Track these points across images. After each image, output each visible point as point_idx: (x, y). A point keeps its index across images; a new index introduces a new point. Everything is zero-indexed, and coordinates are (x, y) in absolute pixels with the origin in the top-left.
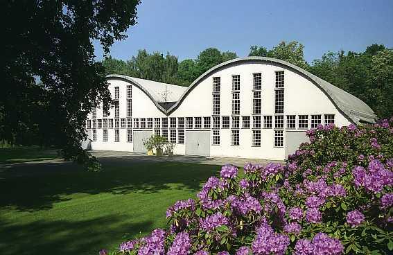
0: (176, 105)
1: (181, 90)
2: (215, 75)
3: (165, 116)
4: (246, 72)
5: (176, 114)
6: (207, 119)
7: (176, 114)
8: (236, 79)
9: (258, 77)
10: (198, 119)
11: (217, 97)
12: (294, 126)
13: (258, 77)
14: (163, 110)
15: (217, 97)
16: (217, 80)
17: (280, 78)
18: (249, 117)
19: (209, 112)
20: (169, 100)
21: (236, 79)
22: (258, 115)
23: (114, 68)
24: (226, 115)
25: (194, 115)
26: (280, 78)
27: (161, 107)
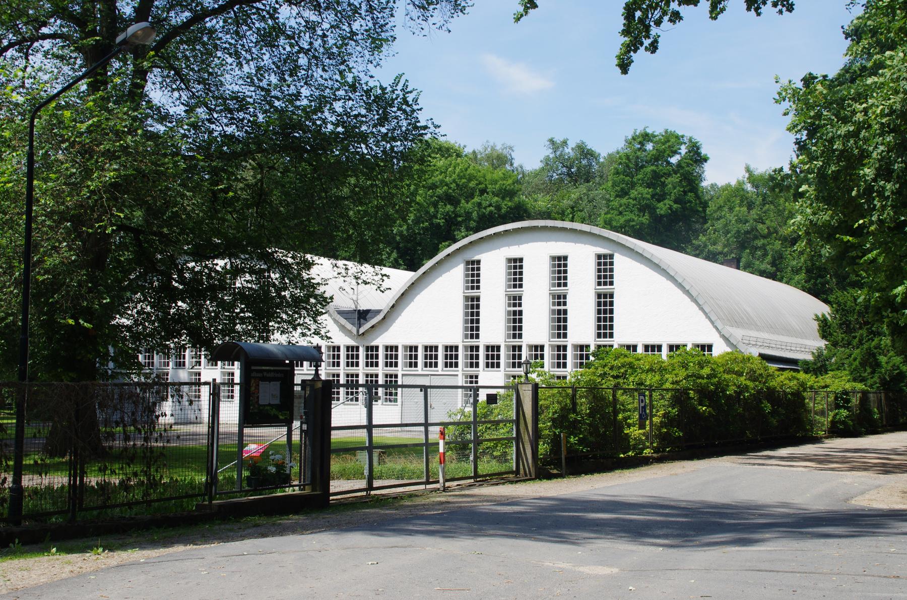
0: (379, 317)
1: (400, 278)
2: (514, 251)
3: (352, 343)
4: (537, 254)
5: (381, 341)
6: (451, 349)
7: (381, 341)
8: (516, 266)
9: (560, 264)
10: (431, 349)
11: (473, 306)
12: (416, 365)
13: (560, 264)
14: (349, 326)
15: (473, 306)
16: (473, 268)
17: (605, 270)
18: (457, 348)
19: (455, 335)
20: (363, 307)
21: (516, 266)
22: (474, 342)
23: (692, 244)
24: (493, 342)
25: (420, 341)
26: (605, 270)
27: (343, 321)
